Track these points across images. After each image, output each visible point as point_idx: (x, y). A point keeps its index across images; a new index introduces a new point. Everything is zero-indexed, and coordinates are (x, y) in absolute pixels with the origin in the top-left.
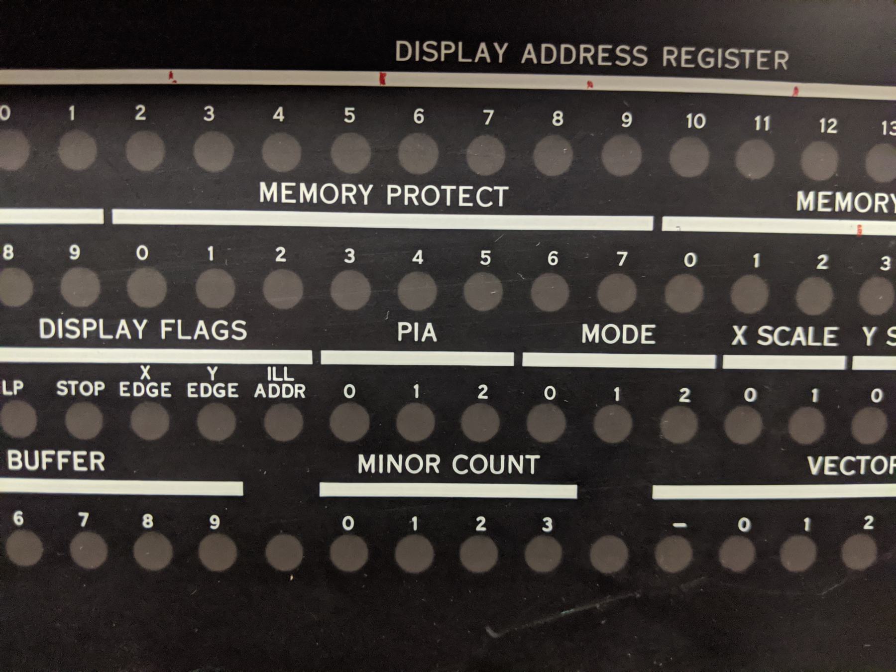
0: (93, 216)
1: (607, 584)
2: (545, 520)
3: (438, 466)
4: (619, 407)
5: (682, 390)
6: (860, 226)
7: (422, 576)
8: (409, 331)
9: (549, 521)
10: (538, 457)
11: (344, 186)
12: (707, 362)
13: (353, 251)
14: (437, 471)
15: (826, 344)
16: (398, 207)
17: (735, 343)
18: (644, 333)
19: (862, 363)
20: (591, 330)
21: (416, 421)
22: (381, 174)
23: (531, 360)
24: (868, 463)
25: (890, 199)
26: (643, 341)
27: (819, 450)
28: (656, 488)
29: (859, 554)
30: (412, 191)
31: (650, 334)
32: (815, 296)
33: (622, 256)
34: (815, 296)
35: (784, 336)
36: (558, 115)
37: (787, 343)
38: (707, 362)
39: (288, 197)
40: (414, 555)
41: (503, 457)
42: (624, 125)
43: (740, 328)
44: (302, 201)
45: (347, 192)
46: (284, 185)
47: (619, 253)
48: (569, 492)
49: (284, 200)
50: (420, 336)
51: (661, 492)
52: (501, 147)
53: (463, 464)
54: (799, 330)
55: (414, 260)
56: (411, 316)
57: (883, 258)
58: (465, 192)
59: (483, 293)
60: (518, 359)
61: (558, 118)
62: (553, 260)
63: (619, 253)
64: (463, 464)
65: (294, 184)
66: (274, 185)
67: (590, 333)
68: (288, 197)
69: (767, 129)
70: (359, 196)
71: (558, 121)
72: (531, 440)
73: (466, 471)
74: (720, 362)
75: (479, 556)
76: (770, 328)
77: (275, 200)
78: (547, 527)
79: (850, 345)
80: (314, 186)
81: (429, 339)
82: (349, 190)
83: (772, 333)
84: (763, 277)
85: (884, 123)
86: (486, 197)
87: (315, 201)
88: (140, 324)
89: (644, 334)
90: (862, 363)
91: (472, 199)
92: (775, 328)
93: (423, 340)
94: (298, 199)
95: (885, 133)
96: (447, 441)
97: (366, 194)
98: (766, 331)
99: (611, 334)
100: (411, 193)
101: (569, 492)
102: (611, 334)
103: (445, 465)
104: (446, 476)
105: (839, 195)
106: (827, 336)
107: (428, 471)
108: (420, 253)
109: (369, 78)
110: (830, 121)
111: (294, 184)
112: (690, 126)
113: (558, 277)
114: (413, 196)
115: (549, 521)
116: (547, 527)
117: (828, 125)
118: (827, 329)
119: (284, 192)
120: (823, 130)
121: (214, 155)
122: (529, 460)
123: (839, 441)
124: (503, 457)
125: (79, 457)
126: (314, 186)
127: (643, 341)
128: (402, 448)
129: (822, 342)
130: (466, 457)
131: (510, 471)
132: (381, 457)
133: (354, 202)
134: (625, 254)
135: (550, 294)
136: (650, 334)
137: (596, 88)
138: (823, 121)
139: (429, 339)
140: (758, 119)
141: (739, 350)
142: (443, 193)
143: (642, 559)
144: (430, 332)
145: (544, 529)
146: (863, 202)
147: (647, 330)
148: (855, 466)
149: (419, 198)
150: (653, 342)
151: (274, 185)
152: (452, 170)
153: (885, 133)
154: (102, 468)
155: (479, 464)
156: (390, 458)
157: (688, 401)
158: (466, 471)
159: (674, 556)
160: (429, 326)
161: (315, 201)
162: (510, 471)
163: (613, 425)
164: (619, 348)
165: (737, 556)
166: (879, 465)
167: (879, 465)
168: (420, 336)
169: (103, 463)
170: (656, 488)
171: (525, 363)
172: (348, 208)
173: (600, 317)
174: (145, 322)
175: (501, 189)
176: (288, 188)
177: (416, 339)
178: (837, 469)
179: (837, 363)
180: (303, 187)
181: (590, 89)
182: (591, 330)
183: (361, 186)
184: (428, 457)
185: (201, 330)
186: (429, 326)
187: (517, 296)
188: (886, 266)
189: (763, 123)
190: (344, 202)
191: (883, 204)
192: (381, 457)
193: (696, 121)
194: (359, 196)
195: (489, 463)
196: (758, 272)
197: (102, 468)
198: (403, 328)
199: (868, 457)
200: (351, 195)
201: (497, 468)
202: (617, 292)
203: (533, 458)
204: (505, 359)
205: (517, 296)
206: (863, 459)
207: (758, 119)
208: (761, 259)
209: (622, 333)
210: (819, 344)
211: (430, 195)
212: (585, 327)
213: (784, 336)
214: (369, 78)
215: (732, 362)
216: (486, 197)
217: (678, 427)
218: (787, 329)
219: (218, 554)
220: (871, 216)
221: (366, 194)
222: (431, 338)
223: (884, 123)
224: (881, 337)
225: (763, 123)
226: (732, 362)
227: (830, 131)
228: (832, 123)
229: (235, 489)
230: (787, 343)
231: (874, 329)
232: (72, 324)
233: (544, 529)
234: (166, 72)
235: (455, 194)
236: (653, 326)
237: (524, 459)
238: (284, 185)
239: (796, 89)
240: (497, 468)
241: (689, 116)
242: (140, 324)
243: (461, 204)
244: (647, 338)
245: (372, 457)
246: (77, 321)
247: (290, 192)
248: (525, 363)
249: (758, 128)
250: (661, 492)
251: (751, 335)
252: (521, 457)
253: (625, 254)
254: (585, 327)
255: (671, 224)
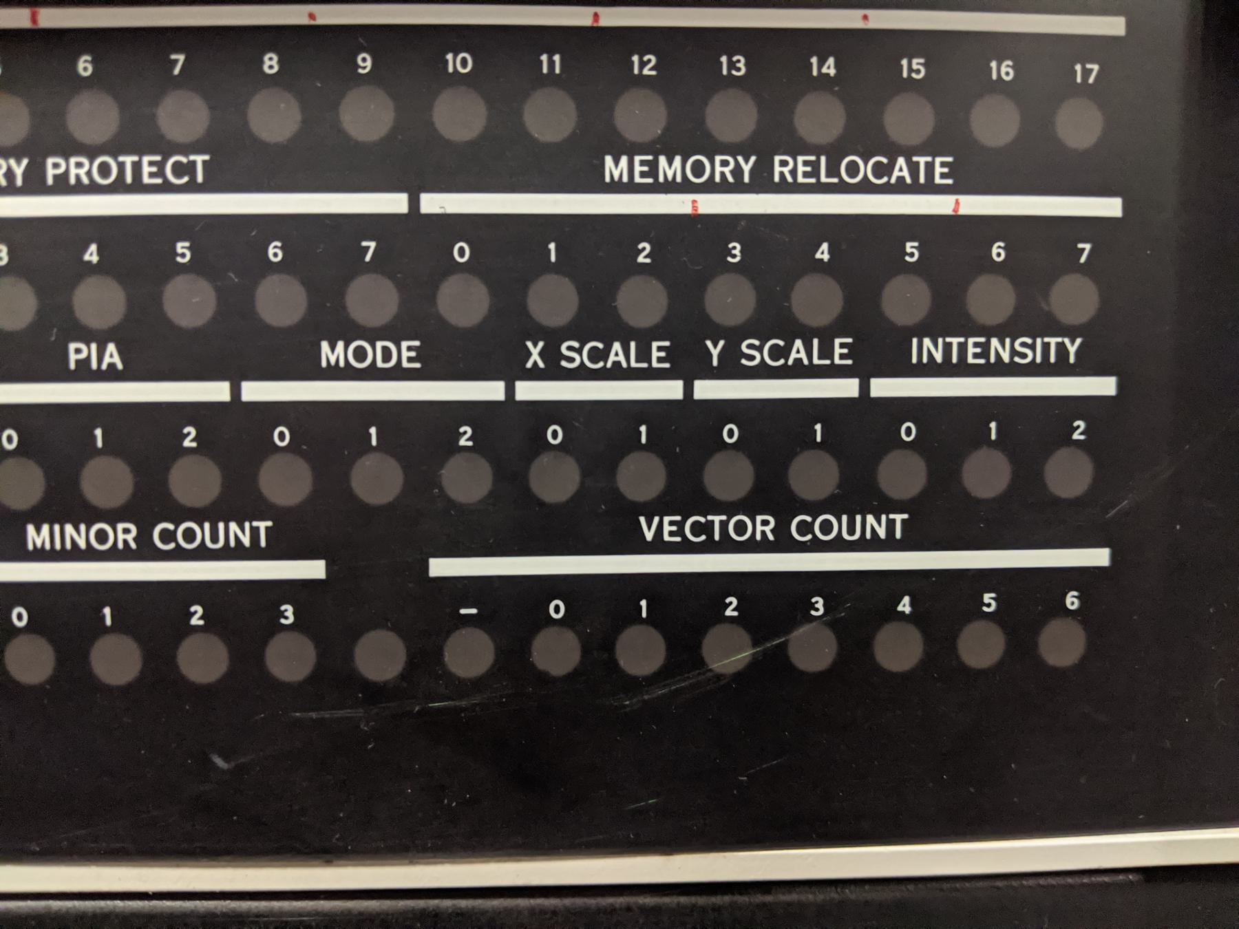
0: (394, 203)
1: (374, 693)
2: (283, 608)
3: (135, 539)
4: (289, 457)
5: (462, 430)
6: (694, 202)
7: (126, 690)
8: (83, 355)
9: (288, 610)
10: (269, 524)
11: (718, 159)
12: (492, 391)
13: (738, 246)
14: (771, 537)
15: (655, 364)
16: (62, 186)
17: (529, 365)
18: (406, 352)
19: (706, 390)
20: (333, 349)
21: (107, 480)
22: (769, 140)
23: (253, 391)
24: (724, 525)
25: (737, 162)
26: (405, 364)
27: (654, 509)
28: (433, 562)
29: (1062, 646)
30: (79, 165)
31: (845, 351)
32: (642, 301)
33: (368, 248)
34: (816, 299)
35: (595, 355)
36: (271, 59)
37: (601, 364)
38: (492, 391)
39: (643, 174)
40: (116, 661)
41: (221, 526)
42: (360, 71)
43: (535, 345)
44: (661, 179)
45: (721, 167)
46: (637, 159)
47: (364, 244)
48: (314, 569)
49: (638, 179)
50: (100, 360)
51: (440, 567)
52: (391, 105)
53: (167, 536)
54: (617, 346)
55: (818, 256)
56: (86, 336)
57: (731, 246)
58: (151, 164)
59: (189, 303)
60: (236, 391)
61: (271, 63)
62: (999, 255)
63: (364, 244)
64: (805, 528)
65: (650, 158)
66: (624, 160)
67: (332, 354)
68: (643, 174)
69: (557, 71)
70: (737, 172)
71: (271, 67)
72: (261, 497)
73: (809, 537)
74: (510, 391)
75: (813, 649)
76: (576, 344)
77: (625, 179)
78: (286, 618)
79: (687, 364)
80: (678, 160)
81: (112, 366)
82: (725, 163)
83: (760, 349)
84: (565, 274)
85: (724, 59)
86: (179, 170)
87: (679, 179)
88: (715, 346)
89: (405, 354)
90: (706, 390)
91: (161, 173)
92: (763, 341)
93: (104, 367)
94: (656, 177)
95: (725, 72)
96: (150, 506)
97: (747, 168)
98: (570, 348)
99: (360, 354)
100: (78, 168)
101: (314, 569)
102: (360, 354)
103: (144, 537)
104: (145, 551)
105: (663, 160)
106: (655, 354)
107: (758, 537)
108: (825, 246)
109: (579, 17)
110: (646, 58)
111: (650, 158)
112: (451, 70)
113: (284, 277)
114: (786, 170)
115: (288, 610)
116: (286, 618)
117: (643, 64)
118: (655, 345)
119: (638, 169)
120: (636, 71)
121: (550, 119)
122: (258, 528)
123: (686, 495)
124: (858, 518)
125: (671, 523)
126: (678, 160)
127: (405, 364)
128: (86, 514)
129: (650, 362)
130: (809, 519)
131: (868, 536)
132: (57, 528)
133: (731, 179)
134: (373, 245)
135: (280, 303)
136: (845, 351)
137: (320, 21)
138: (635, 58)
139: (112, 366)
140: (544, 58)
141: (535, 375)
142: (121, 166)
143: (424, 659)
144: (112, 355)
145: (283, 621)
146: (698, 169)
147: (409, 349)
148: (707, 528)
149: (89, 173)
150: (849, 362)
151: (624, 160)
152: (138, 136)
153: (725, 72)
154: (133, 545)
155: (189, 535)
156: (69, 528)
157: (470, 444)
158: (809, 537)
159: (470, 654)
160: (111, 347)
161: (679, 179)
162: (868, 536)
163: (377, 480)
164: (373, 374)
165: (898, 650)
166: (740, 529)
167: (740, 529)
168: (100, 360)
169: (135, 539)
170: (433, 562)
171: (520, 396)
172: (723, 187)
173: (346, 331)
174: (721, 343)
175: (199, 159)
176: (642, 163)
177: (94, 365)
178: (680, 532)
179: (672, 390)
180: (663, 160)
181: (312, 23)
182: (333, 349)
183: (740, 159)
184: (759, 518)
185: (111, 356)
186: (111, 347)
187: (236, 305)
188: (734, 256)
189: (551, 64)
190: (717, 179)
191: (727, 170)
192: (57, 528)
193: (646, 65)
194: (737, 172)
195: (202, 533)
196: (557, 269)
197: (133, 545)
198: (76, 352)
199: (724, 518)
200: (727, 170)
201: (851, 531)
202: (372, 298)
203: (262, 525)
204: (218, 391)
205: (236, 305)
206: (717, 519)
207: (544, 58)
208: (562, 60)
209: (375, 353)
210: (645, 365)
211: (104, 170)
212: (325, 346)
213: (595, 355)
214: (579, 17)
215: (527, 391)
216: (179, 170)
217: (467, 481)
218: (600, 346)
219: (289, 659)
220: (710, 187)
221: (747, 168)
222: (801, 360)
223: (724, 59)
224: (552, 355)
225: (551, 64)
226: (527, 391)
227: (646, 72)
228: (649, 61)
229: (1099, 557)
230: (601, 364)
231: (1078, 341)
232: (1024, 345)
233: (283, 621)
234: (860, 13)
235: (137, 167)
236: (667, 344)
237: (252, 528)
238: (637, 159)
239: (596, 16)
240: (215, 539)
241: (450, 57)
242: (715, 346)
243: (938, 180)
244: (410, 360)
245: (45, 528)
246: (1029, 341)
247: (646, 169)
248: (520, 396)
249: (545, 70)
250: (440, 567)
251: (552, 355)
252: (247, 525)
253: (373, 245)
254: (325, 346)
255: (432, 203)
